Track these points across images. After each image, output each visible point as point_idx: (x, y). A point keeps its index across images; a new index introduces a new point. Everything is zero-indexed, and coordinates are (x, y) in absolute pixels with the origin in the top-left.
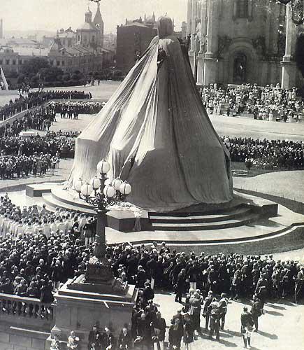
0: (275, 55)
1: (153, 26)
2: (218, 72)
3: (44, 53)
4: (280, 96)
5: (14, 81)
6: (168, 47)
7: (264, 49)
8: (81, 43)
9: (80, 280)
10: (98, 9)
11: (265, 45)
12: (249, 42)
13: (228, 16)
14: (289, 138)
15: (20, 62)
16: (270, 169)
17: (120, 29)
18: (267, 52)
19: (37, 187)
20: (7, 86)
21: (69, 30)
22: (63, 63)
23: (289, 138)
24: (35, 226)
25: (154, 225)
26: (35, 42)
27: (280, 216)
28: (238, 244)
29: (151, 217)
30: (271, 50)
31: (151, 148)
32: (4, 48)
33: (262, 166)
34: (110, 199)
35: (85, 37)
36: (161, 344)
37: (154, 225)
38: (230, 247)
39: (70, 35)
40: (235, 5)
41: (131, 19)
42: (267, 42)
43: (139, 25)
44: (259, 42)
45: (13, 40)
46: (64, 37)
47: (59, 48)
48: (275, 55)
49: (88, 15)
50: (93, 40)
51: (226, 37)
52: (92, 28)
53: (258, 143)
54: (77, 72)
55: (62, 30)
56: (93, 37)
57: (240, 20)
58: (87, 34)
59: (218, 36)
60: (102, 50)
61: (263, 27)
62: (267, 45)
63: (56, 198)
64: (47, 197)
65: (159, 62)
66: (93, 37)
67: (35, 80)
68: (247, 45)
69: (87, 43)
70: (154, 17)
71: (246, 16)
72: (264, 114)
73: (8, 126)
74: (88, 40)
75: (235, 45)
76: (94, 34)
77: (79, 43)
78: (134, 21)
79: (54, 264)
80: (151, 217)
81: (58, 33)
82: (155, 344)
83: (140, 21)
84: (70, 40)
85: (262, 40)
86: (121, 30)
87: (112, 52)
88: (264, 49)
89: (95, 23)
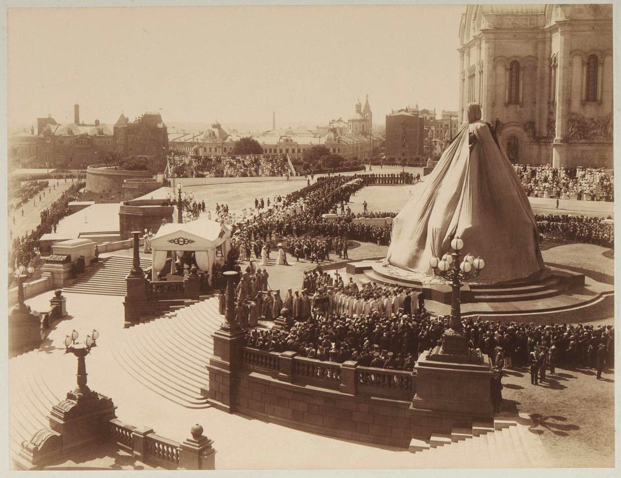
1: (418, 115)
3: (323, 141)
4: (551, 174)
6: (481, 127)
7: (534, 133)
8: (352, 131)
9: (438, 350)
10: (367, 100)
11: (534, 128)
12: (520, 126)
14: (571, 213)
15: (299, 151)
16: (559, 242)
17: (389, 119)
18: (537, 135)
20: (294, 173)
22: (339, 150)
23: (571, 213)
24: (371, 302)
25: (476, 297)
26: (311, 131)
29: (473, 290)
30: (540, 132)
31: (469, 226)
33: (552, 239)
34: (466, 274)
37: (476, 297)
39: (341, 125)
40: (507, 91)
42: (537, 126)
45: (290, 130)
47: (335, 137)
49: (358, 107)
50: (363, 129)
52: (362, 118)
53: (542, 218)
55: (333, 121)
56: (363, 126)
57: (512, 107)
61: (533, 112)
62: (538, 130)
64: (370, 274)
65: (470, 146)
66: (363, 126)
68: (518, 129)
69: (358, 132)
70: (417, 106)
71: (516, 102)
72: (540, 192)
73: (580, 197)
74: (359, 129)
75: (508, 129)
76: (364, 123)
77: (350, 132)
78: (399, 111)
79: (422, 335)
80: (473, 290)
83: (407, 111)
85: (532, 124)
87: (381, 140)
88: (534, 133)
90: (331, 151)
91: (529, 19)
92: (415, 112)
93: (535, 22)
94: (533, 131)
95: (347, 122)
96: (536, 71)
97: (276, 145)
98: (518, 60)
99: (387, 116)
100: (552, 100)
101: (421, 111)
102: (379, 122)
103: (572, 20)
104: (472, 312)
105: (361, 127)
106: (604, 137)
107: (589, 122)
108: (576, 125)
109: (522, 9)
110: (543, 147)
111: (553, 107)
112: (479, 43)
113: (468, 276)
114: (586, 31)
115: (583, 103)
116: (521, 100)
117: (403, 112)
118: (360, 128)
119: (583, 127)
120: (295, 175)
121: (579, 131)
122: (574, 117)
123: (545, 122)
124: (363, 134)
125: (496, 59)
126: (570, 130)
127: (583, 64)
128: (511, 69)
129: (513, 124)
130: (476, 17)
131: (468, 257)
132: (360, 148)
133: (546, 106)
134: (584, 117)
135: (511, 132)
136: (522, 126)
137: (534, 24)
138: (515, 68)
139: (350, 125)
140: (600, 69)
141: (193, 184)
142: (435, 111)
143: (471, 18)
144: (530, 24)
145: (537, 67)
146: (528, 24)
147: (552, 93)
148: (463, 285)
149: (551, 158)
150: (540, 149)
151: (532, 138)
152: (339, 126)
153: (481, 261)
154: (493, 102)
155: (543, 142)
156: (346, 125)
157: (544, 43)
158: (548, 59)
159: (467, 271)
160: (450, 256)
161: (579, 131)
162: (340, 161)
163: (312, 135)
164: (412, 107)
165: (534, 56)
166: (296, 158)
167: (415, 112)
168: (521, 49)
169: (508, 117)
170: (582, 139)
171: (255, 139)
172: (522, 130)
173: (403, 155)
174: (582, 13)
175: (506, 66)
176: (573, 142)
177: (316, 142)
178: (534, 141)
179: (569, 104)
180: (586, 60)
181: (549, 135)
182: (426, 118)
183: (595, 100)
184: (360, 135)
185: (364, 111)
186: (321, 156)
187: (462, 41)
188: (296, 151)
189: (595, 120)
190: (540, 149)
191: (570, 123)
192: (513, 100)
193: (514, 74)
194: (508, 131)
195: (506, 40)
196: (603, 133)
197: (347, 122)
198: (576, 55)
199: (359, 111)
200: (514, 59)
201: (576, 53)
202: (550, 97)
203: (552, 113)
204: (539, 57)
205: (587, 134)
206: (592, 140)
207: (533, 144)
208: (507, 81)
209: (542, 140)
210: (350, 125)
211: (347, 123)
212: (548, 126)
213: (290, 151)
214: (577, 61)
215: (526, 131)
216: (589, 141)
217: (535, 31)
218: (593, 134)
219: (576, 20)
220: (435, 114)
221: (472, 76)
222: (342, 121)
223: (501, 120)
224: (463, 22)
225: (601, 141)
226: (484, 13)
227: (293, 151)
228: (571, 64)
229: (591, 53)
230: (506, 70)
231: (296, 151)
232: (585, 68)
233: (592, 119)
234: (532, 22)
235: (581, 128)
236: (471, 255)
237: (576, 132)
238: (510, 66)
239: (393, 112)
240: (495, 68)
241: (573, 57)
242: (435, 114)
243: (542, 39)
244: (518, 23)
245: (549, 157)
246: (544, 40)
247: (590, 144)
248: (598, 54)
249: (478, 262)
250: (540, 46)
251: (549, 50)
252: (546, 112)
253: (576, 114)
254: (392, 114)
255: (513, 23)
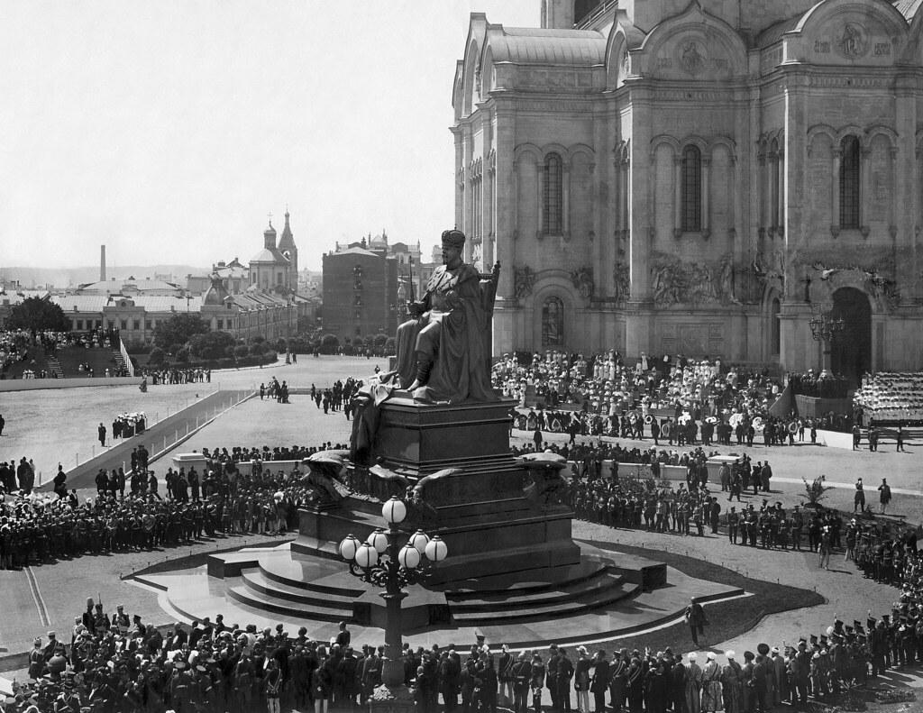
0: (612, 300)
1: (385, 253)
2: (516, 332)
3: (196, 305)
5: (144, 359)
10: (287, 224)
12: (565, 277)
13: (529, 231)
15: (148, 325)
17: (328, 260)
18: (597, 294)
19: (230, 558)
21: (235, 263)
22: (229, 323)
25: (456, 617)
26: (174, 285)
27: (671, 586)
28: (612, 641)
30: (603, 290)
32: (115, 298)
35: (266, 274)
36: (326, 702)
37: (456, 617)
38: (309, 542)
39: (237, 273)
41: (344, 242)
42: (597, 276)
43: (358, 250)
44: (583, 276)
45: (132, 282)
46: (227, 276)
48: (612, 300)
49: (270, 236)
50: (280, 280)
51: (527, 270)
54: (260, 340)
55: (222, 264)
56: (280, 274)
57: (550, 239)
58: (269, 270)
59: (514, 267)
60: (297, 299)
62: (598, 285)
63: (270, 576)
64: (255, 577)
67: (183, 357)
68: (562, 282)
70: (385, 237)
71: (558, 232)
78: (350, 246)
81: (215, 269)
82: (317, 704)
83: (363, 245)
84: (237, 281)
85: (588, 272)
86: (333, 263)
88: (592, 288)
89: (282, 248)
90: (214, 326)
91: (576, 75)
92: (380, 248)
93: (588, 82)
94: (589, 287)
95: (248, 266)
96: (592, 172)
97: (100, 313)
98: (560, 151)
99: (325, 255)
100: (622, 228)
101: (393, 246)
102: (310, 264)
103: (652, 79)
104: (648, 624)
105: (276, 277)
106: (717, 298)
107: (688, 270)
108: (666, 276)
109: (572, 53)
110: (608, 317)
111: (625, 241)
112: (488, 118)
113: (412, 576)
114: (677, 101)
115: (678, 235)
116: (566, 228)
117: (357, 248)
118: (273, 279)
119: (678, 280)
120: (132, 374)
121: (671, 287)
122: (661, 260)
123: (611, 269)
124: (278, 292)
125: (517, 149)
126: (655, 285)
127: (675, 160)
128: (547, 168)
129: (553, 272)
130: (480, 68)
131: (417, 537)
132: (271, 320)
133: (612, 239)
134: (679, 261)
135: (550, 288)
136: (570, 276)
137: (585, 85)
138: (554, 165)
139: (254, 274)
140: (705, 171)
141: (41, 387)
142: (419, 246)
143: (473, 71)
144: (579, 85)
145: (595, 164)
146: (576, 84)
147: (622, 214)
148: (406, 595)
149: (622, 339)
150: (602, 321)
151: (588, 301)
152: (233, 276)
153: (441, 543)
154: (515, 231)
155: (608, 308)
156: (246, 274)
157: (605, 120)
158: (614, 151)
159: (412, 567)
160: (383, 536)
161: (671, 287)
162: (226, 345)
163: (175, 293)
164: (376, 235)
165: (590, 145)
166: (143, 339)
167: (380, 248)
168: (559, 129)
169: (543, 260)
170: (676, 301)
171: (55, 300)
172: (570, 285)
173: (358, 332)
174: (671, 67)
175: (536, 163)
176: (662, 307)
177: (182, 306)
178: (592, 305)
179: (652, 236)
180: (680, 154)
181: (619, 296)
182: (402, 261)
183: (697, 227)
184: (273, 292)
185: (280, 245)
186: (190, 335)
187: (458, 114)
188: (142, 326)
189: (700, 266)
190: (602, 321)
191: (654, 272)
192: (554, 225)
193: (552, 178)
194: (543, 285)
195: (536, 114)
196: (714, 291)
197: (248, 266)
198: (663, 144)
199: (270, 245)
200: (551, 149)
201: (660, 141)
202: (618, 223)
203: (622, 253)
204: (597, 147)
205: (686, 292)
206: (695, 306)
207: (590, 311)
208: (540, 189)
209: (607, 304)
210: (254, 274)
211: (246, 269)
212: (616, 277)
213: (130, 325)
214: (664, 156)
215: (576, 285)
216: (689, 307)
217: (588, 97)
218: (698, 292)
219: (659, 80)
220: (420, 253)
221: (476, 181)
222: (239, 265)
223: (531, 266)
224: (460, 76)
225: (711, 306)
226: (494, 61)
227: (136, 325)
228: (653, 160)
229: (689, 142)
230: (538, 169)
231: (142, 326)
232: (678, 168)
233: (694, 265)
234: (583, 81)
235: (675, 281)
236: (421, 533)
237: (665, 290)
238: (545, 162)
239: (338, 247)
240: (516, 166)
241: (656, 149)
242: (420, 253)
243: (602, 112)
244: (557, 81)
245: (619, 336)
246: (604, 114)
247: (691, 311)
248: (700, 144)
249: (436, 547)
250: (598, 126)
251: (614, 134)
252: (612, 256)
253: (665, 255)
254: (337, 251)
255: (549, 82)
